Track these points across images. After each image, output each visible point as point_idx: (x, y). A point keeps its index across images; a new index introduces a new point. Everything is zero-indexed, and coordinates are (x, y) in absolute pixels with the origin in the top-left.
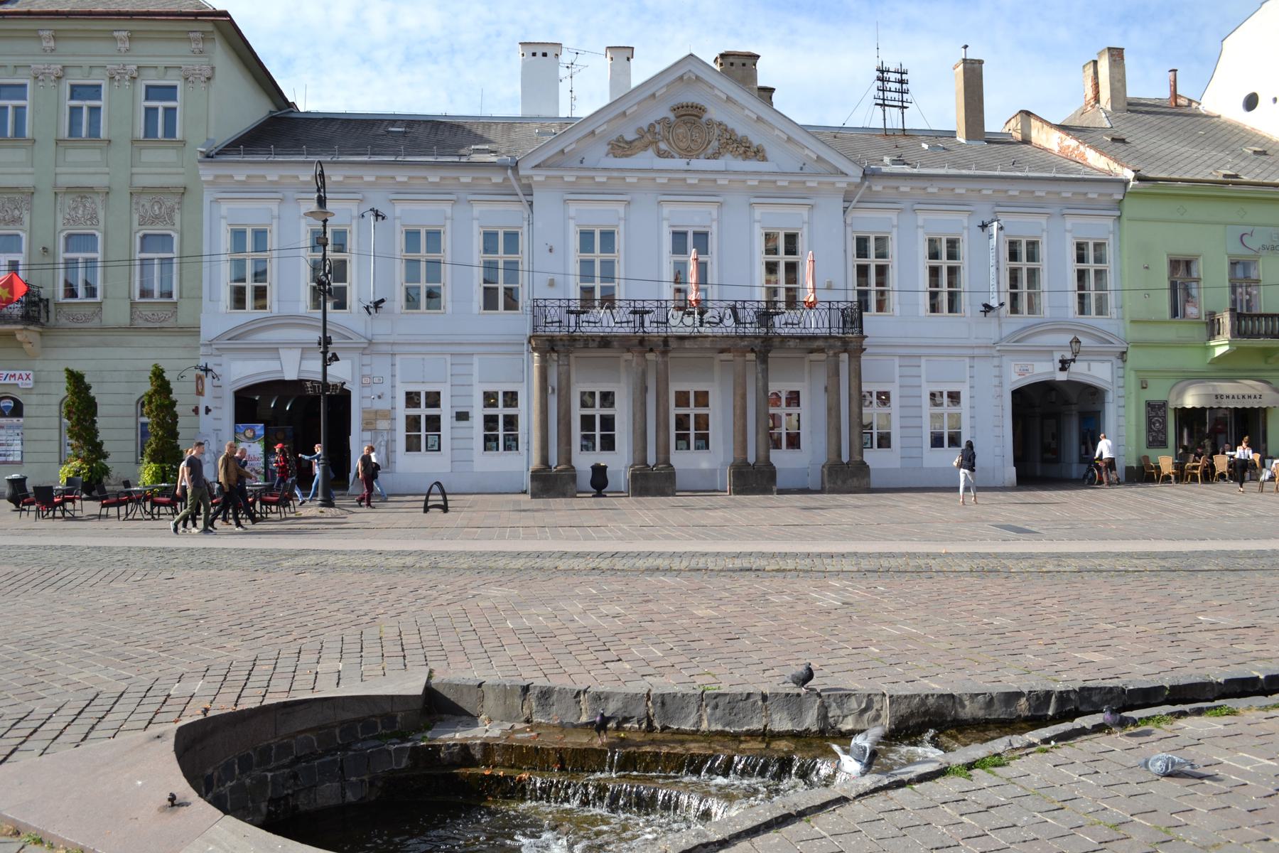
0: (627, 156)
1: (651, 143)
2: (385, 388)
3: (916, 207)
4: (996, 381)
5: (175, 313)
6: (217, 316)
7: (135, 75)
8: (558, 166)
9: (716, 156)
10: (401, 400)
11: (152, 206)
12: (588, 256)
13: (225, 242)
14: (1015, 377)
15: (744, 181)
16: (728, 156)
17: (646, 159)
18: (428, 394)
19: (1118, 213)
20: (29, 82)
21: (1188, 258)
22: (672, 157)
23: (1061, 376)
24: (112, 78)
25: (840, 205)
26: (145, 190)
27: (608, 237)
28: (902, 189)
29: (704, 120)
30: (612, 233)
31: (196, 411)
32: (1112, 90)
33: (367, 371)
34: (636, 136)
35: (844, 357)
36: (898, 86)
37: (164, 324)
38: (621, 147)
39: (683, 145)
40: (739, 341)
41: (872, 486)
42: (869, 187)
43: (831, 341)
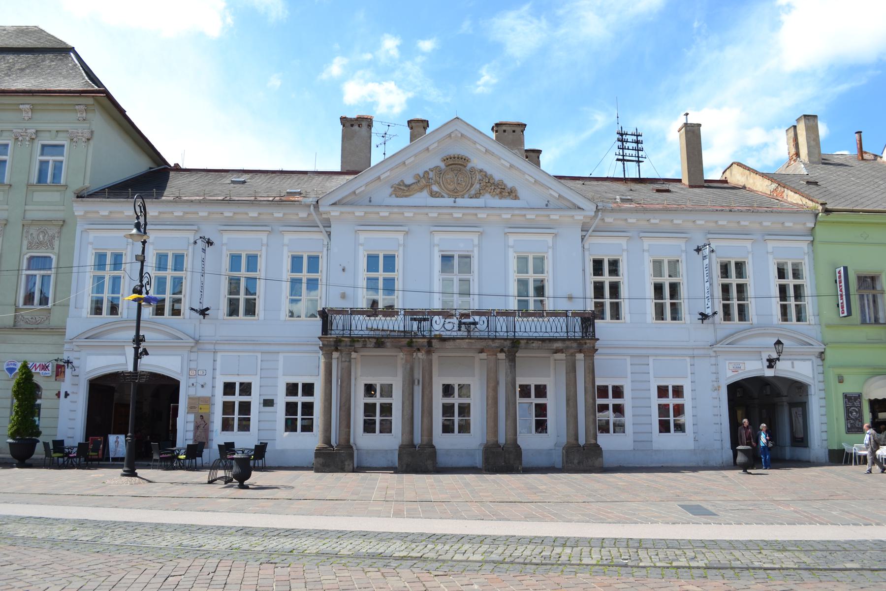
0: (406, 196)
1: (426, 186)
2: (207, 379)
3: (642, 235)
4: (714, 377)
5: (48, 318)
6: (79, 318)
7: (33, 137)
8: (352, 204)
9: (477, 196)
10: (220, 389)
11: (38, 235)
12: (373, 275)
13: (91, 260)
14: (730, 374)
15: (500, 215)
16: (487, 196)
17: (422, 198)
18: (241, 384)
19: (811, 238)
20: (11, 143)
21: (872, 274)
22: (443, 197)
23: (769, 373)
24: (17, 139)
25: (579, 234)
26: (34, 222)
27: (390, 262)
28: (630, 221)
29: (468, 168)
30: (393, 257)
31: (58, 395)
32: (809, 147)
33: (193, 365)
34: (414, 181)
35: (580, 356)
36: (635, 145)
37: (39, 326)
38: (402, 189)
39: (451, 187)
40: (490, 342)
41: (606, 465)
42: (603, 220)
43: (567, 343)
